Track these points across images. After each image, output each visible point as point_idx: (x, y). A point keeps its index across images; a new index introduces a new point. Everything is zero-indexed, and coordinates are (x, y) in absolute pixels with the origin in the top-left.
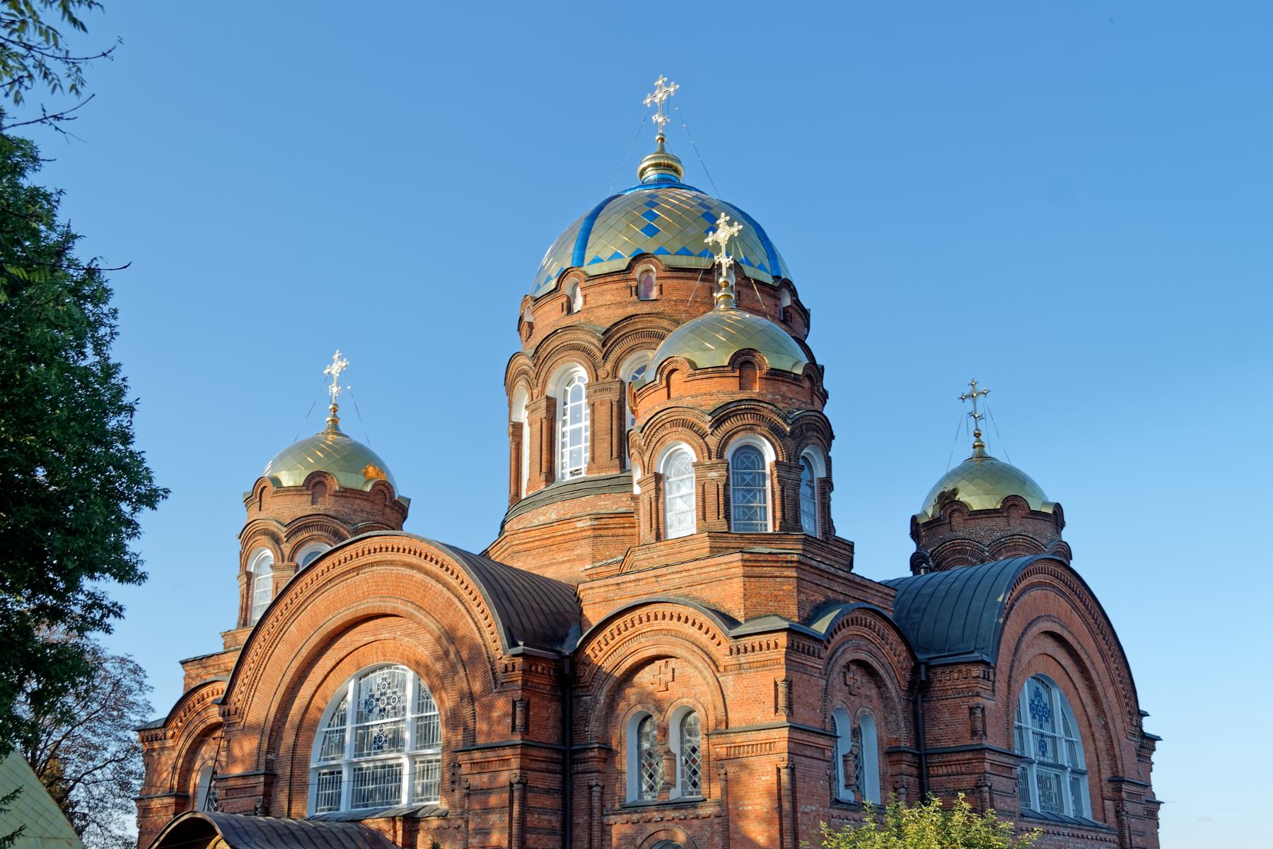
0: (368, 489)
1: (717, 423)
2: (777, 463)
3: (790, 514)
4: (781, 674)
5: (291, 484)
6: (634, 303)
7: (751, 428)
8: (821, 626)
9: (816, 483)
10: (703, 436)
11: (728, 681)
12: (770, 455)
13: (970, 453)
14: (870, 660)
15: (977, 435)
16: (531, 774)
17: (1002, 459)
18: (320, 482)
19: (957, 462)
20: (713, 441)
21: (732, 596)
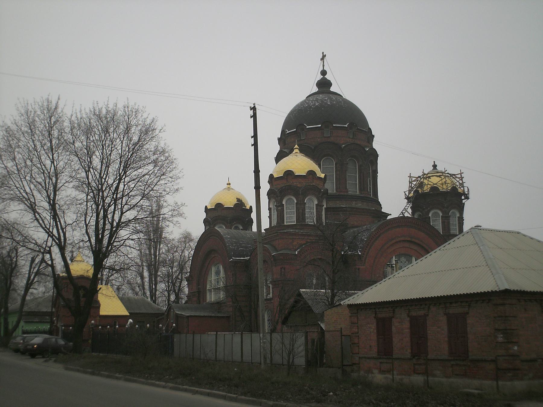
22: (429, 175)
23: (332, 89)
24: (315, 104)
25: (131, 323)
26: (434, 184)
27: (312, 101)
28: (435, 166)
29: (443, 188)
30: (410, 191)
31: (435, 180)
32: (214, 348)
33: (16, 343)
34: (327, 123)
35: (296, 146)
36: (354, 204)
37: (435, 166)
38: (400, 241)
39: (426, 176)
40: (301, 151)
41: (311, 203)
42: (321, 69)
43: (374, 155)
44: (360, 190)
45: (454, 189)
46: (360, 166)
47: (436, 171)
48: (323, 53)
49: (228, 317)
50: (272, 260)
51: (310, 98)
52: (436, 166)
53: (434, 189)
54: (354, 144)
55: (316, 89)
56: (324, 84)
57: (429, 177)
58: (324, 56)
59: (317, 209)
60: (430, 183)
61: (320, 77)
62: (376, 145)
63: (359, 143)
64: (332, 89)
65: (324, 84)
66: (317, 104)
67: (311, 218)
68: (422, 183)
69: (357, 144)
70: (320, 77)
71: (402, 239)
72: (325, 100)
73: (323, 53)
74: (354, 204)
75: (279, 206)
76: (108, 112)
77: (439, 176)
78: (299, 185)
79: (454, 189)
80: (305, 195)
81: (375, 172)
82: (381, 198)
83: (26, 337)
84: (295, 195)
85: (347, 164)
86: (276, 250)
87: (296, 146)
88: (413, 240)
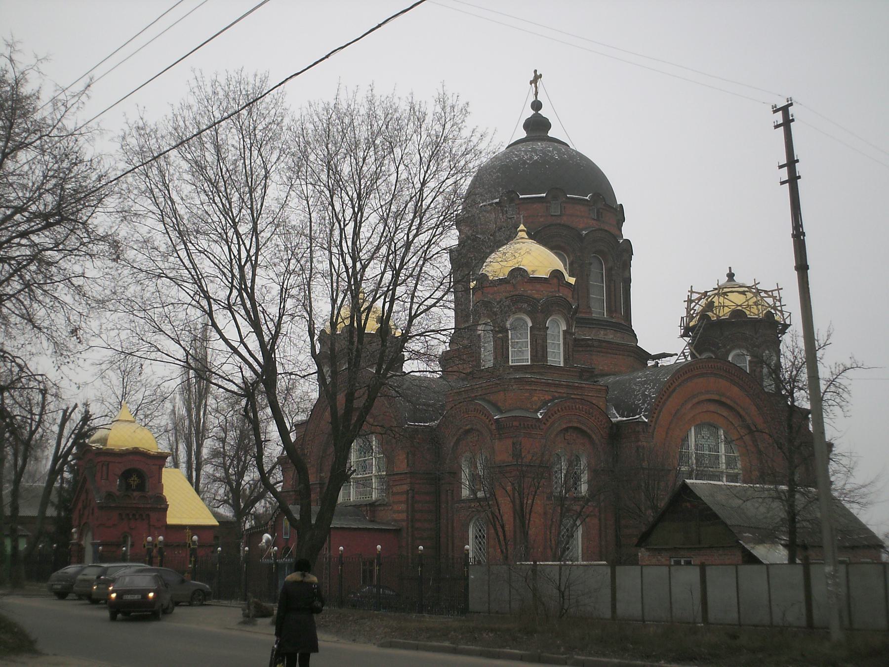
9: (561, 333)
12: (530, 324)
14: (579, 425)
22: (726, 290)
23: (551, 134)
24: (531, 158)
25: (268, 541)
26: (738, 306)
27: (526, 152)
28: (731, 276)
29: (754, 313)
30: (691, 318)
31: (737, 299)
32: (640, 587)
33: (84, 580)
34: (556, 192)
35: (522, 227)
36: (601, 335)
37: (731, 276)
38: (703, 401)
39: (720, 291)
40: (531, 237)
41: (557, 329)
42: (533, 99)
43: (626, 249)
44: (610, 311)
45: (769, 315)
46: (609, 270)
47: (733, 283)
48: (535, 71)
49: (398, 531)
50: (494, 427)
51: (520, 146)
52: (734, 275)
53: (738, 313)
54: (601, 230)
55: (523, 134)
56: (537, 126)
57: (725, 294)
58: (537, 78)
59: (564, 339)
60: (727, 303)
61: (531, 113)
62: (627, 232)
63: (606, 228)
64: (551, 134)
65: (537, 126)
66: (536, 158)
67: (556, 356)
68: (712, 303)
69: (606, 231)
70: (531, 113)
71: (707, 397)
72: (549, 151)
73: (535, 71)
74: (601, 335)
75: (500, 332)
76: (371, 116)
77: (743, 293)
78: (536, 296)
79: (769, 315)
80: (547, 313)
81: (628, 281)
82: (637, 325)
83: (108, 568)
84: (530, 314)
85: (591, 264)
86: (500, 411)
87: (522, 227)
88: (723, 399)
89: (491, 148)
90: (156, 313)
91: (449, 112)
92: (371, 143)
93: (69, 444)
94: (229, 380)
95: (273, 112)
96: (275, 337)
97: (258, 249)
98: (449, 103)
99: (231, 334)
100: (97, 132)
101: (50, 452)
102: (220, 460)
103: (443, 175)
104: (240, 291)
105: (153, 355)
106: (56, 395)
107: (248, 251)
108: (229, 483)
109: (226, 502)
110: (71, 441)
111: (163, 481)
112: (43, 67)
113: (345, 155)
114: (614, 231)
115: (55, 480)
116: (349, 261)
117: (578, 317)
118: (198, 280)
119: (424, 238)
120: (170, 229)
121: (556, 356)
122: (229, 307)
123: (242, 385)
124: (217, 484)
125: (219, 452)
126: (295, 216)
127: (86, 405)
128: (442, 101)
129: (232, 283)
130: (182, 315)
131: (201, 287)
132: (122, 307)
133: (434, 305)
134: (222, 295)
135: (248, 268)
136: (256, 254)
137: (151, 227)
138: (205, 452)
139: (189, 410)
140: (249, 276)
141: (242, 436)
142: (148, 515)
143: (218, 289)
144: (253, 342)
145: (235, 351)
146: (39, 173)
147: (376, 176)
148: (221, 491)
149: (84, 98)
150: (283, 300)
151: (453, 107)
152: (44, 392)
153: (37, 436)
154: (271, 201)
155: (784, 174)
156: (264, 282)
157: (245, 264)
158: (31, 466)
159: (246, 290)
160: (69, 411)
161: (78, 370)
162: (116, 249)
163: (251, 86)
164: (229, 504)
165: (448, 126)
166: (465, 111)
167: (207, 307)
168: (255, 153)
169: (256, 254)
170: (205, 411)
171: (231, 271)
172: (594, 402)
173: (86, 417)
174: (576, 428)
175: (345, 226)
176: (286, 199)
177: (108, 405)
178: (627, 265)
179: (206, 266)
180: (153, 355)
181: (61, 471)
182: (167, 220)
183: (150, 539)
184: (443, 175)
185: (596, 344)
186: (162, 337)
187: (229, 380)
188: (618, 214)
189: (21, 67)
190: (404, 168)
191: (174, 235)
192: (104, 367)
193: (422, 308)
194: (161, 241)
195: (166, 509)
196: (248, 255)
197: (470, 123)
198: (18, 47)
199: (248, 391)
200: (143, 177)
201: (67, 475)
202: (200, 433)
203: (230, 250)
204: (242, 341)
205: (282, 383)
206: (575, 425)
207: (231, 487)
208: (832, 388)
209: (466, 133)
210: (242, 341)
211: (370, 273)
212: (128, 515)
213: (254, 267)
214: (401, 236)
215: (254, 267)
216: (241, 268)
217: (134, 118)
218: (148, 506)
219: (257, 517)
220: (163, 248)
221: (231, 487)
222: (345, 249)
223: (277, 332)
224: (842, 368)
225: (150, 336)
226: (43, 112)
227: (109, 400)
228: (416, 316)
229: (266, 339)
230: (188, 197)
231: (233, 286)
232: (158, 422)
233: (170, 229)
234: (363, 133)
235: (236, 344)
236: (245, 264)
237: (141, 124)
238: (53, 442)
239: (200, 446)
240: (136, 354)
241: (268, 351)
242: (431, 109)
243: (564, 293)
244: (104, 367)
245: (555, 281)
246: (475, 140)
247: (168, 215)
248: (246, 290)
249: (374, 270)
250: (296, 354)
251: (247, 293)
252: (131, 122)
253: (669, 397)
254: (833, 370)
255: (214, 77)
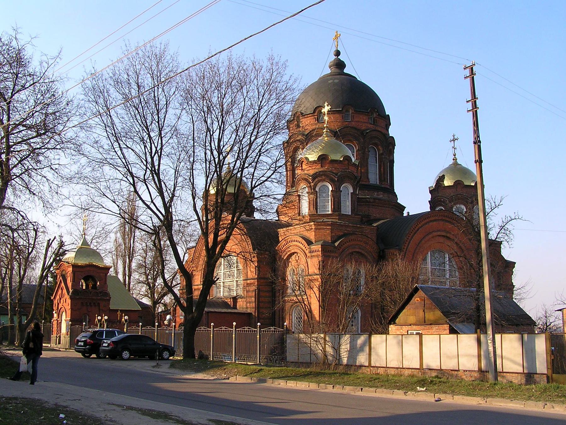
0: (342, 159)
1: (313, 179)
2: (331, 191)
3: (336, 206)
4: (320, 259)
5: (313, 159)
6: (316, 124)
7: (323, 180)
8: (336, 244)
9: (350, 194)
10: (310, 183)
11: (309, 260)
12: (331, 189)
13: (452, 162)
14: (360, 251)
15: (455, 155)
16: (261, 287)
17: (464, 165)
18: (324, 158)
19: (447, 166)
20: (312, 184)
21: (311, 236)
23: (346, 71)
43: (390, 144)
58: (337, 37)
62: (392, 132)
63: (379, 130)
64: (346, 71)
69: (379, 131)
81: (392, 162)
89: (299, 87)
90: (102, 185)
91: (276, 67)
92: (229, 85)
93: (51, 260)
94: (145, 225)
95: (171, 65)
96: (172, 199)
97: (162, 146)
98: (276, 60)
99: (146, 197)
100: (66, 79)
101: (40, 265)
102: (143, 270)
103: (272, 103)
104: (151, 171)
105: (100, 210)
106: (44, 232)
107: (156, 148)
108: (148, 284)
109: (146, 296)
110: (52, 258)
111: (108, 283)
112: (34, 41)
113: (212, 93)
114: (384, 131)
115: (43, 282)
116: (215, 153)
117: (361, 184)
118: (127, 165)
119: (260, 141)
120: (110, 135)
121: (347, 208)
122: (145, 181)
123: (152, 228)
124: (140, 285)
125: (142, 265)
126: (185, 127)
127: (61, 236)
128: (271, 59)
129: (146, 166)
130: (118, 186)
131: (128, 170)
132: (81, 181)
133: (266, 180)
134: (141, 174)
135: (156, 158)
136: (161, 149)
137: (99, 133)
138: (134, 265)
139: (124, 239)
140: (156, 163)
141: (155, 258)
142: (99, 303)
143: (138, 171)
144: (159, 202)
145: (149, 207)
146: (32, 102)
147: (233, 103)
148: (144, 289)
149: (58, 60)
150: (176, 178)
151: (277, 63)
152: (36, 231)
153: (32, 255)
154: (170, 119)
155: (470, 106)
156: (165, 167)
157: (154, 155)
158: (29, 273)
159: (155, 170)
160: (51, 241)
161: (57, 216)
162: (79, 149)
163: (158, 49)
164: (148, 296)
165: (275, 74)
166: (285, 66)
167: (132, 181)
168: (160, 90)
169: (161, 149)
170: (134, 240)
171: (146, 161)
172: (369, 236)
173: (62, 244)
174: (358, 252)
175: (213, 133)
176: (180, 118)
177: (74, 236)
178: (392, 152)
179: (131, 157)
180: (100, 210)
181: (47, 276)
182: (108, 129)
183: (99, 318)
184: (272, 103)
185: (371, 200)
186: (105, 199)
187: (145, 225)
188: (386, 120)
189: (21, 43)
190: (244, 103)
191: (113, 139)
192: (71, 217)
193: (258, 183)
194: (105, 143)
195: (109, 300)
196: (156, 150)
197: (288, 72)
198: (19, 31)
199: (156, 232)
200: (94, 104)
201: (50, 279)
202: (130, 253)
203: (145, 147)
204: (152, 202)
205: (176, 227)
206: (357, 250)
207: (149, 286)
208: (503, 231)
209: (286, 78)
210: (152, 202)
211: (227, 161)
212: (90, 303)
213: (160, 157)
214: (246, 141)
215: (160, 157)
216: (152, 158)
217: (89, 69)
218: (99, 298)
219: (165, 305)
220: (106, 147)
221: (149, 286)
222: (213, 148)
223: (173, 195)
224: (509, 219)
225: (97, 199)
226: (34, 66)
227: (75, 233)
228: (255, 187)
229: (166, 200)
230: (122, 117)
231: (147, 168)
232: (105, 247)
233: (110, 135)
234: (224, 78)
235: (148, 203)
236: (154, 155)
237: (93, 72)
238: (42, 257)
239: (130, 261)
240: (90, 209)
241: (167, 207)
242: (266, 64)
243: (352, 169)
244: (71, 217)
245: (347, 162)
246: (291, 82)
247: (110, 126)
248: (156, 172)
249: (230, 159)
250: (185, 210)
251: (156, 173)
252: (88, 71)
253: (415, 233)
254: (504, 220)
255: (136, 45)
